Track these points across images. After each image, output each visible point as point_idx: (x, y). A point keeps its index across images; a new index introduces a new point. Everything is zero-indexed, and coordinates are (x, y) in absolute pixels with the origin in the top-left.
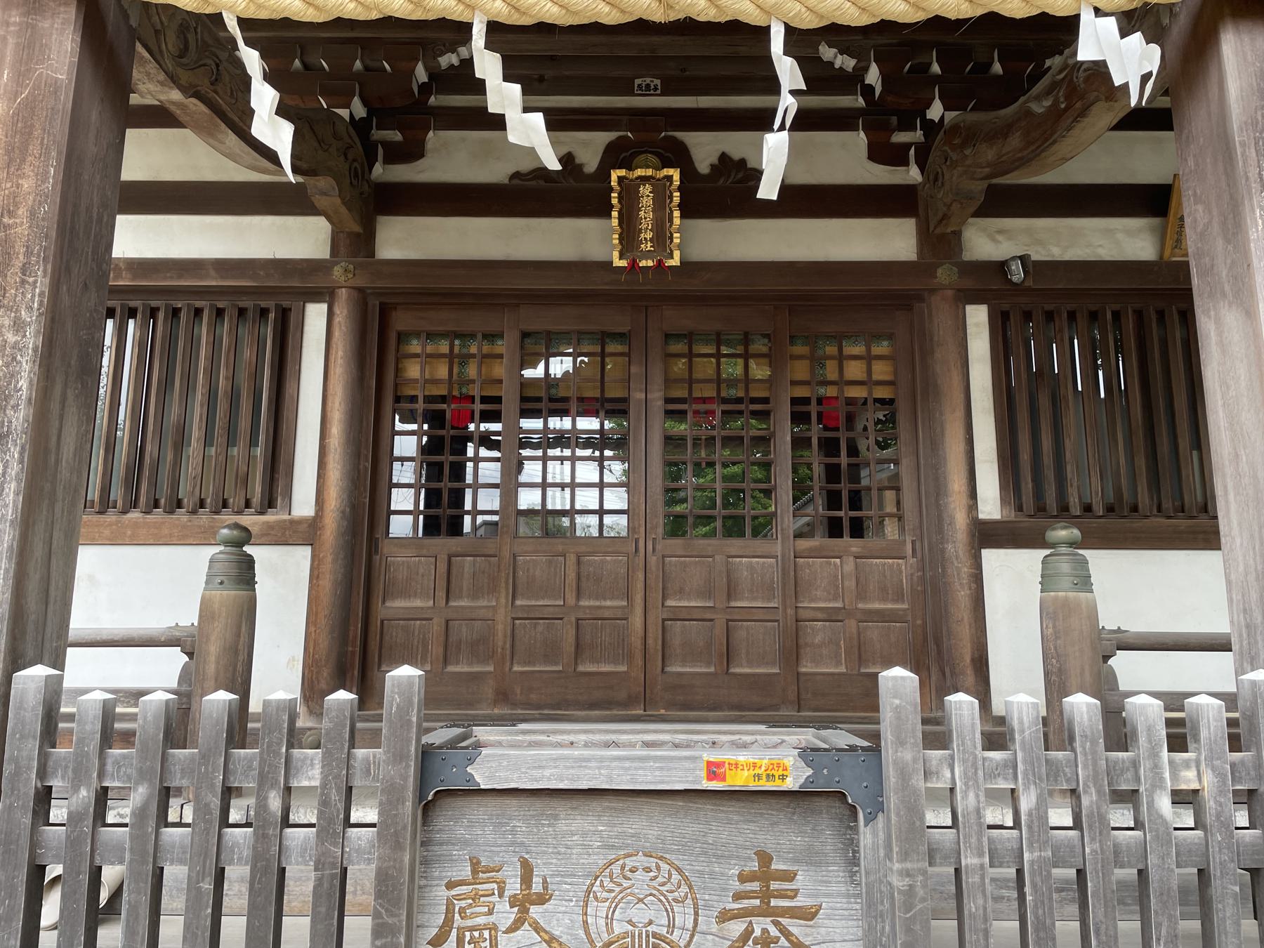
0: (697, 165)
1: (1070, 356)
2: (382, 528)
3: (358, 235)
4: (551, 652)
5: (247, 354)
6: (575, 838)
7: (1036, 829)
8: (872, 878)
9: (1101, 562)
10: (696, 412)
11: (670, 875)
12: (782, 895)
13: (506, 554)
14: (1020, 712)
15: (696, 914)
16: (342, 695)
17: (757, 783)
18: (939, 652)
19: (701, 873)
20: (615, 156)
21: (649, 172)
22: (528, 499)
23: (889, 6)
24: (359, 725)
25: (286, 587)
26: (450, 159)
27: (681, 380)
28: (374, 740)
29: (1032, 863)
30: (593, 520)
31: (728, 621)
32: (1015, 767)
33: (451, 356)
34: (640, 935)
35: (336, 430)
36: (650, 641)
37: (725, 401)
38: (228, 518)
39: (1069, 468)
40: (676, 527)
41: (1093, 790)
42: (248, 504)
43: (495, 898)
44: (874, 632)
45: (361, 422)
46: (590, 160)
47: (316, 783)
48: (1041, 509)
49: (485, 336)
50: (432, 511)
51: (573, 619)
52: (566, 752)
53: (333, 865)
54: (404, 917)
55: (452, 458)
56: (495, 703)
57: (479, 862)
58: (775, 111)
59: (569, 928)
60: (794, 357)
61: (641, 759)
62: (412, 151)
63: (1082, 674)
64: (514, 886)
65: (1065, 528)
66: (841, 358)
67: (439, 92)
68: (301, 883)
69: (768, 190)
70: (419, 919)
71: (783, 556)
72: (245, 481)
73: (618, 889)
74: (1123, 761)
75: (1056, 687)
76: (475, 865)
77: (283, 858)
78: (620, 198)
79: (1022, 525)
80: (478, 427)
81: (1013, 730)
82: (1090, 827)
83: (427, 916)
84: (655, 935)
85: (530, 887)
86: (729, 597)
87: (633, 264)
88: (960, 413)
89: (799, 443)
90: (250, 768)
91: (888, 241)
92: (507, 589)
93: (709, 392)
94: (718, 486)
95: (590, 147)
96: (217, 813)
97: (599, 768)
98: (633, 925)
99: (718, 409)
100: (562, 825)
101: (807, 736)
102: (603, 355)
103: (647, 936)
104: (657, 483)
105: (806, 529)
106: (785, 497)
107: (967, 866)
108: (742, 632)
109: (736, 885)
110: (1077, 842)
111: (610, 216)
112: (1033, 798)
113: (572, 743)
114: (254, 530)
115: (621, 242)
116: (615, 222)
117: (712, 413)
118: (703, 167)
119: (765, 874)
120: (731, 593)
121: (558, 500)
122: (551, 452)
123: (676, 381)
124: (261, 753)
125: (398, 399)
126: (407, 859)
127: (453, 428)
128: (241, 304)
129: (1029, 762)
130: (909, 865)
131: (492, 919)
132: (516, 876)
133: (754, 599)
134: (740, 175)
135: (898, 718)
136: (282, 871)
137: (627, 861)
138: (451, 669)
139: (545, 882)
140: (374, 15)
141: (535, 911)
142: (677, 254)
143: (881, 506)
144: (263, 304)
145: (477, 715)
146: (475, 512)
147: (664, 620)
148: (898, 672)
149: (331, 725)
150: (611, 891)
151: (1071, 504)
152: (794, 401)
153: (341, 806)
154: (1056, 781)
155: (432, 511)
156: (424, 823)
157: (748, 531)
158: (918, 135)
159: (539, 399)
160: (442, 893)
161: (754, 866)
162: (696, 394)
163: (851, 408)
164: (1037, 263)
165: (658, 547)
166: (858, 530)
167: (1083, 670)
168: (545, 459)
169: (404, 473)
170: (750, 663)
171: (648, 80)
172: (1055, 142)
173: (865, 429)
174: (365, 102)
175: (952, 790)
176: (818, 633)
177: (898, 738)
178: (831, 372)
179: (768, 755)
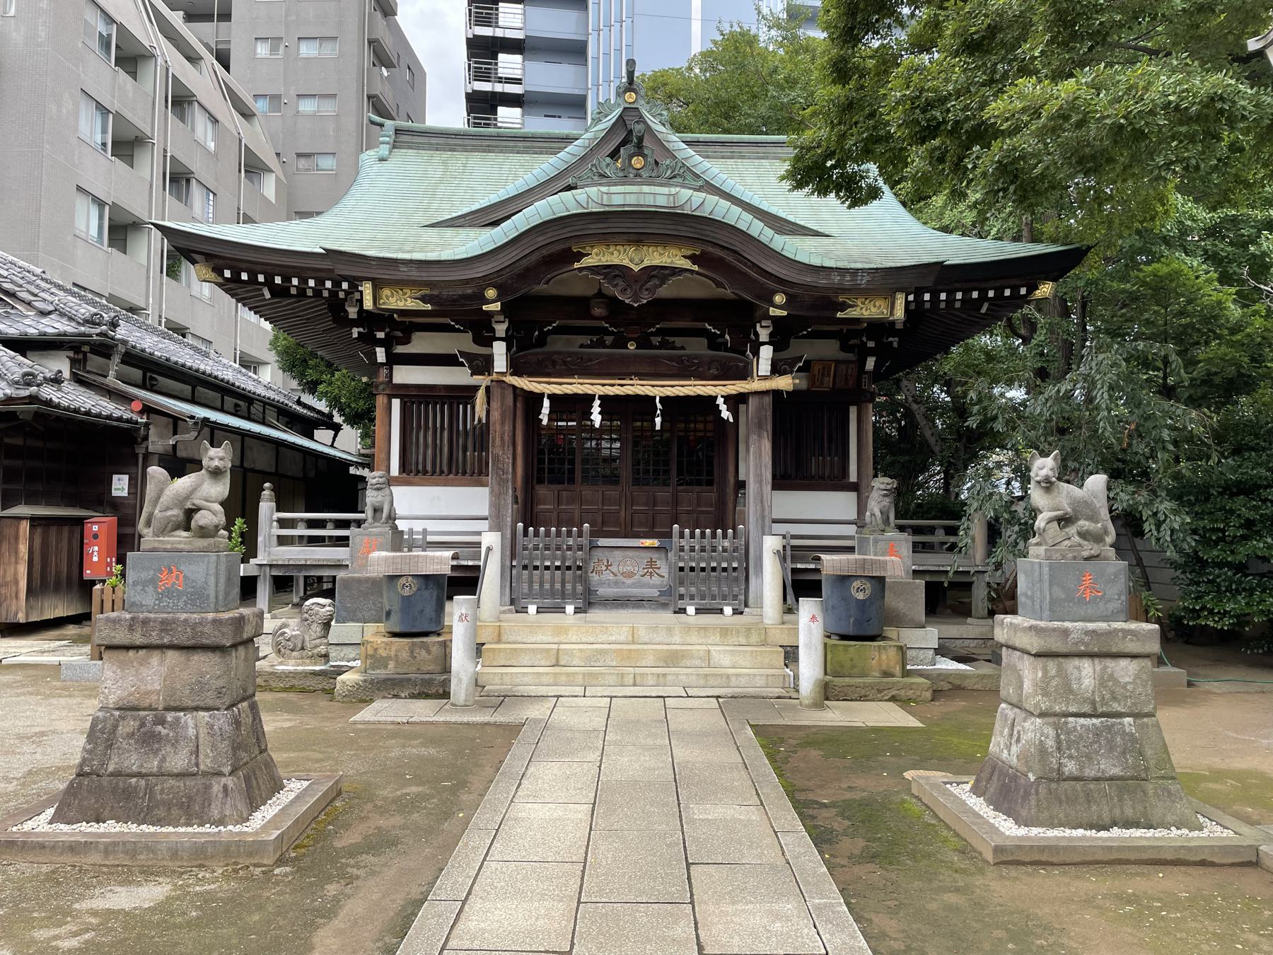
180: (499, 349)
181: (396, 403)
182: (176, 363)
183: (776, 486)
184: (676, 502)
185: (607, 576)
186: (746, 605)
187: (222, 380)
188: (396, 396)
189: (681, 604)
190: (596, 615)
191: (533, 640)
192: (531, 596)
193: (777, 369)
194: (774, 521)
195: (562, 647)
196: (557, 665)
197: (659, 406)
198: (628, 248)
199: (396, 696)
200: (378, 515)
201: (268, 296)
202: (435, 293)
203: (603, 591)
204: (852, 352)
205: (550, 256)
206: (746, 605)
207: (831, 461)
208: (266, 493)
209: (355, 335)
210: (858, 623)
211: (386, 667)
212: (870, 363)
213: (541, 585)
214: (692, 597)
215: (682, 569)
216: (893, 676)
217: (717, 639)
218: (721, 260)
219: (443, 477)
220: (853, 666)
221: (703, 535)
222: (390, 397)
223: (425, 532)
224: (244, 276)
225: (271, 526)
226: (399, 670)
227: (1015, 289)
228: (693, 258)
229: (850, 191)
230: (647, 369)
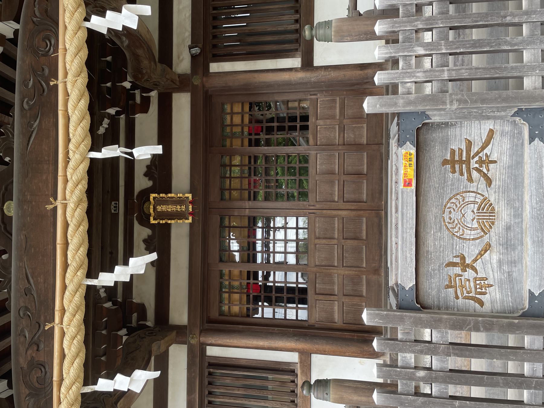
0: (149, 186)
1: (230, 28)
2: (304, 323)
3: (177, 333)
4: (357, 251)
5: (228, 381)
6: (437, 244)
7: (432, 47)
8: (453, 117)
9: (319, 16)
10: (255, 187)
11: (453, 203)
12: (461, 155)
13: (315, 269)
14: (383, 54)
15: (469, 192)
16: (375, 344)
17: (413, 165)
18: (357, 84)
19: (451, 190)
20: (144, 221)
21: (152, 207)
22: (292, 260)
23: (82, 107)
24: (389, 337)
25: (330, 366)
26: (146, 295)
27: (241, 193)
28: (394, 330)
29: (447, 49)
30: (300, 231)
31: (344, 174)
32: (406, 56)
33: (230, 293)
34: (478, 216)
35: (261, 343)
36: (353, 208)
37: (250, 175)
38: (299, 390)
39: (279, 29)
40: (304, 195)
41: (416, 23)
42: (293, 381)
43: (463, 278)
44: (349, 112)
45: (258, 332)
46: (146, 232)
47: (413, 355)
48: (297, 41)
49: (221, 278)
50: (297, 301)
51: (343, 241)
52: (400, 247)
53: (448, 348)
54: (471, 318)
55: (274, 293)
56: (379, 275)
57: (447, 285)
58: (126, 158)
59: (475, 246)
60: (231, 145)
61: (403, 215)
62: (141, 309)
63: (367, 25)
64: (458, 270)
65: (305, 32)
66: (232, 125)
67: (116, 297)
68: (455, 362)
69: (159, 150)
70: (471, 311)
71: (316, 150)
72: (283, 382)
73: (459, 225)
74: (403, 10)
75: (371, 36)
76: (448, 287)
77: (445, 370)
78: (163, 219)
79: (303, 48)
80: (260, 281)
81: (390, 57)
82: (431, 24)
83: (470, 308)
84: (478, 209)
85: (458, 263)
86: (334, 174)
87: (191, 214)
88: (256, 75)
89: (268, 143)
90: (406, 384)
91: (182, 105)
92: (330, 269)
93: (246, 181)
94: (286, 178)
95: (141, 233)
96: (426, 399)
97: (407, 233)
98: (474, 219)
99: (253, 178)
100: (431, 249)
101: (393, 143)
102: (230, 227)
103: (479, 213)
104: (286, 204)
105: (305, 139)
106: (291, 150)
107: (448, 77)
108: (349, 168)
109: (457, 175)
110: (438, 30)
111: (170, 224)
112: (419, 48)
113: (396, 243)
114: (304, 379)
115: (181, 219)
116: (173, 222)
117: (255, 180)
118: (150, 184)
119: (452, 162)
120: (332, 173)
121: (292, 247)
122: (271, 250)
123: (241, 196)
124: (400, 379)
125: (248, 316)
126: (445, 316)
127: (260, 292)
128: (207, 383)
129: (404, 50)
130: (448, 101)
131: (471, 280)
132: (453, 269)
133: (335, 163)
134: (153, 168)
135: (385, 105)
136: (451, 371)
137: (446, 221)
138: (364, 294)
139: (455, 257)
140: (83, 327)
141: (468, 261)
142: (187, 195)
143: (295, 108)
144: (207, 374)
145: (385, 283)
146: (297, 282)
147: (344, 202)
148: (365, 105)
149: (388, 349)
150: (459, 228)
151: (295, 28)
152: (250, 145)
153: (423, 345)
154: (412, 39)
155: (297, 301)
156: (430, 308)
157: (305, 165)
158: (137, 92)
159: (249, 255)
160: (460, 301)
161: (448, 167)
162: (247, 187)
163: (253, 122)
164: (192, 42)
165: (312, 204)
166: (305, 118)
167: (365, 25)
168: (274, 252)
169: (280, 313)
170: (362, 165)
171: (112, 207)
172: (141, 35)
173: (262, 115)
174: (120, 329)
175: (416, 83)
176: (349, 136)
177: (394, 105)
178: (237, 130)
179: (401, 160)
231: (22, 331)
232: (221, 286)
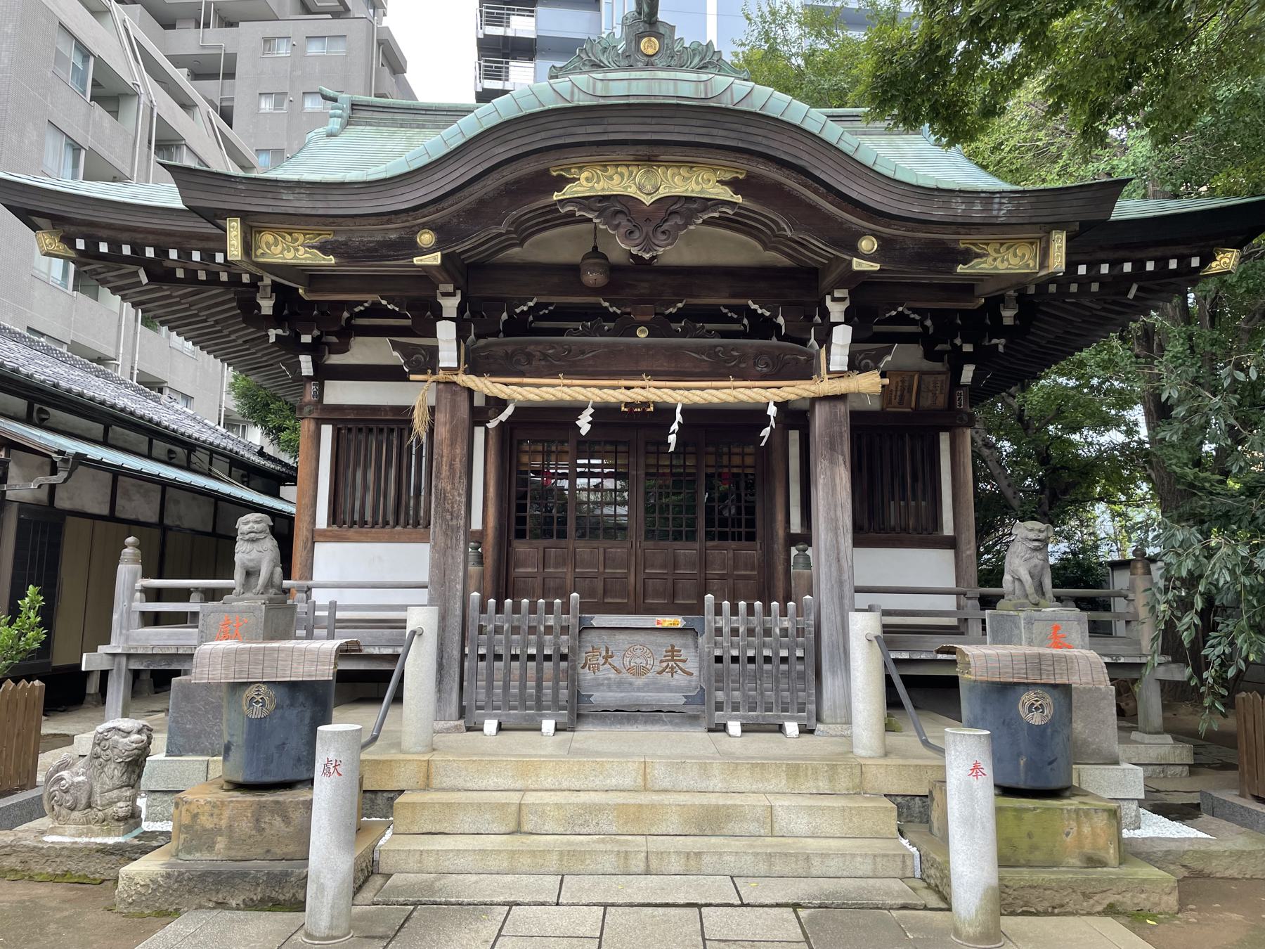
33: (543, 452)
44: (741, 584)
60: (707, 453)
66: (730, 454)
119: (673, 650)
120: (675, 567)
180: (446, 332)
181: (327, 431)
182: (92, 399)
183: (857, 543)
184: (704, 563)
185: (606, 673)
186: (819, 719)
187: (142, 417)
188: (326, 421)
189: (718, 717)
190: (590, 736)
191: (483, 785)
192: (489, 706)
193: (855, 365)
194: (859, 590)
195: (531, 798)
196: (517, 831)
197: (679, 417)
198: (635, 169)
199: (221, 905)
200: (252, 580)
201: (145, 280)
202: (341, 238)
203: (600, 697)
204: (941, 360)
205: (517, 181)
206: (819, 719)
207: (917, 507)
208: (128, 552)
209: (272, 339)
210: (1032, 766)
211: (211, 848)
212: (968, 374)
213: (506, 687)
214: (735, 707)
215: (719, 659)
216: (1102, 863)
217: (782, 783)
218: (778, 188)
219: (387, 529)
220: (1033, 848)
221: (750, 610)
222: (320, 422)
223: (333, 606)
224: (104, 248)
225: (132, 599)
226: (233, 854)
227: (1184, 260)
228: (735, 185)
229: (948, 120)
230: (665, 366)
231: (553, 348)
232: (550, 442)
